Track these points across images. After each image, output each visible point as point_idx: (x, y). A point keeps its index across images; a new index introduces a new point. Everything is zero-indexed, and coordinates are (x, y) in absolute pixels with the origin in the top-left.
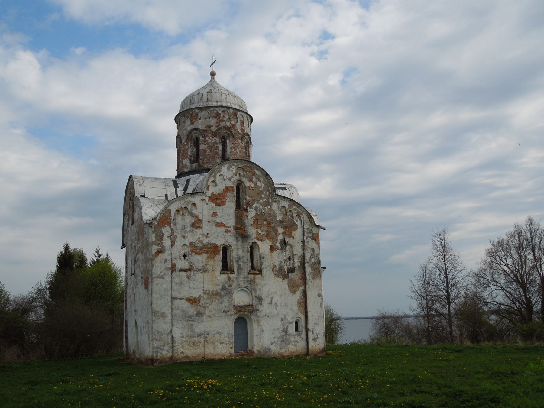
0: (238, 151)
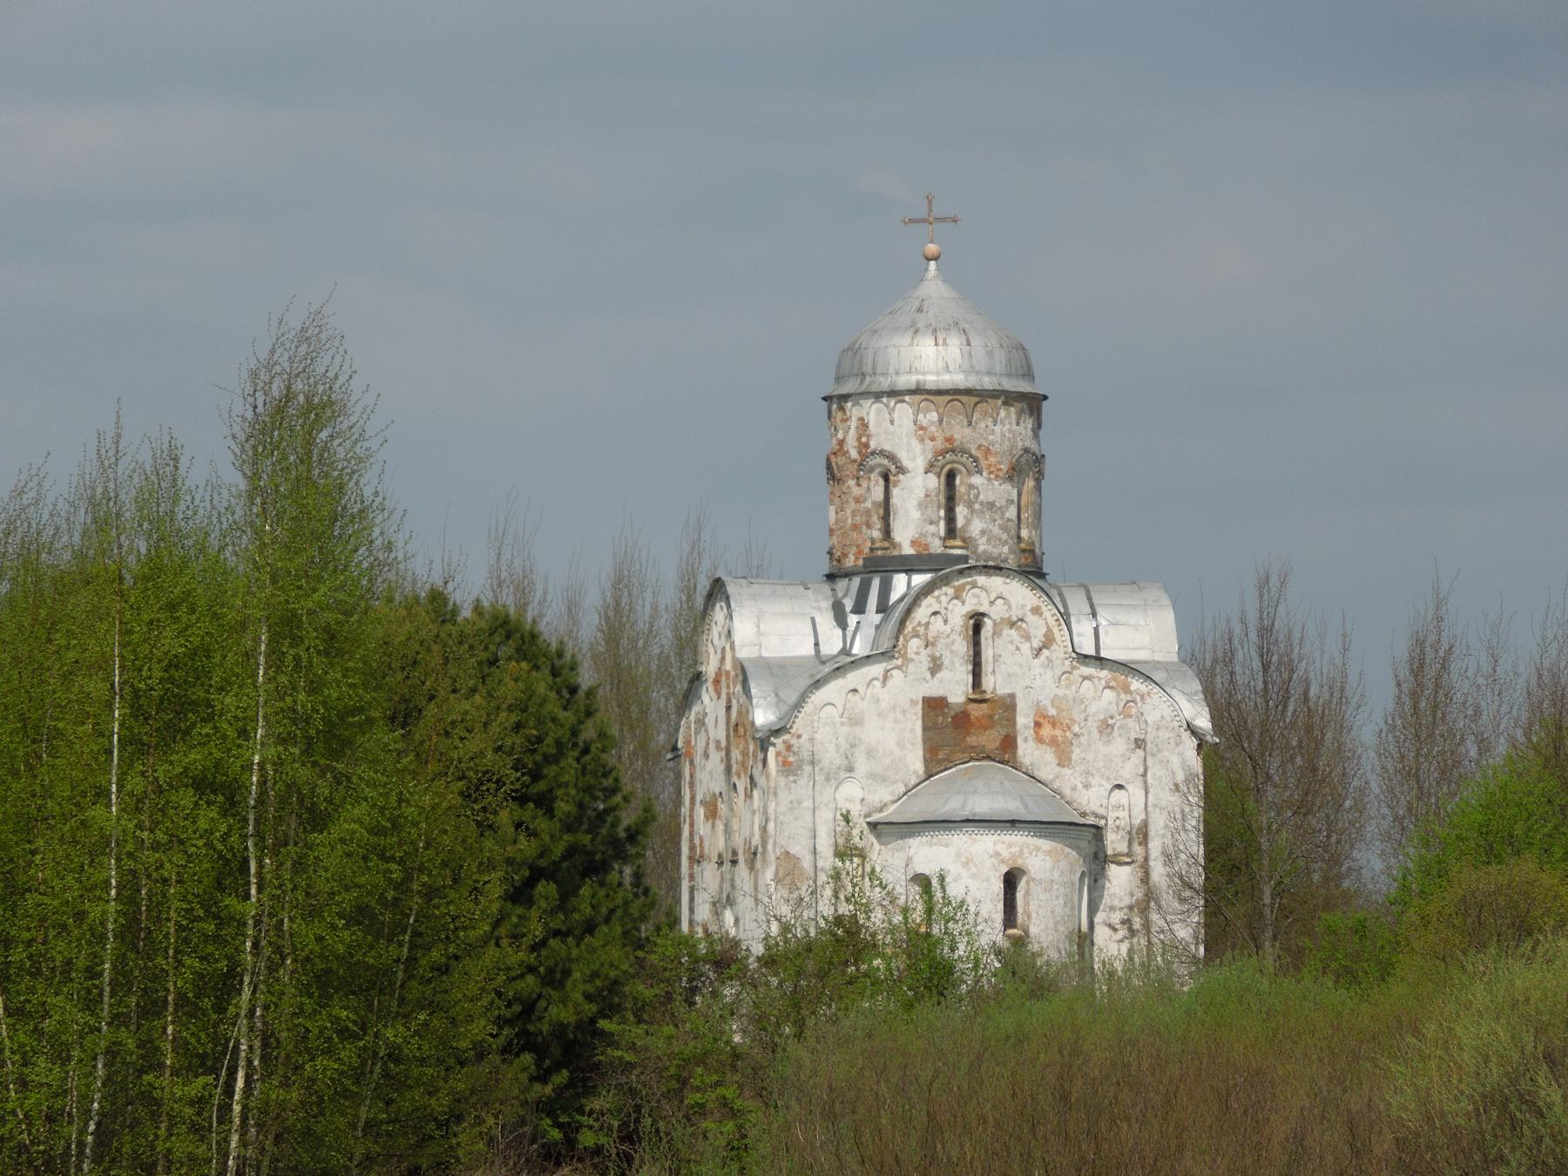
0: (849, 512)
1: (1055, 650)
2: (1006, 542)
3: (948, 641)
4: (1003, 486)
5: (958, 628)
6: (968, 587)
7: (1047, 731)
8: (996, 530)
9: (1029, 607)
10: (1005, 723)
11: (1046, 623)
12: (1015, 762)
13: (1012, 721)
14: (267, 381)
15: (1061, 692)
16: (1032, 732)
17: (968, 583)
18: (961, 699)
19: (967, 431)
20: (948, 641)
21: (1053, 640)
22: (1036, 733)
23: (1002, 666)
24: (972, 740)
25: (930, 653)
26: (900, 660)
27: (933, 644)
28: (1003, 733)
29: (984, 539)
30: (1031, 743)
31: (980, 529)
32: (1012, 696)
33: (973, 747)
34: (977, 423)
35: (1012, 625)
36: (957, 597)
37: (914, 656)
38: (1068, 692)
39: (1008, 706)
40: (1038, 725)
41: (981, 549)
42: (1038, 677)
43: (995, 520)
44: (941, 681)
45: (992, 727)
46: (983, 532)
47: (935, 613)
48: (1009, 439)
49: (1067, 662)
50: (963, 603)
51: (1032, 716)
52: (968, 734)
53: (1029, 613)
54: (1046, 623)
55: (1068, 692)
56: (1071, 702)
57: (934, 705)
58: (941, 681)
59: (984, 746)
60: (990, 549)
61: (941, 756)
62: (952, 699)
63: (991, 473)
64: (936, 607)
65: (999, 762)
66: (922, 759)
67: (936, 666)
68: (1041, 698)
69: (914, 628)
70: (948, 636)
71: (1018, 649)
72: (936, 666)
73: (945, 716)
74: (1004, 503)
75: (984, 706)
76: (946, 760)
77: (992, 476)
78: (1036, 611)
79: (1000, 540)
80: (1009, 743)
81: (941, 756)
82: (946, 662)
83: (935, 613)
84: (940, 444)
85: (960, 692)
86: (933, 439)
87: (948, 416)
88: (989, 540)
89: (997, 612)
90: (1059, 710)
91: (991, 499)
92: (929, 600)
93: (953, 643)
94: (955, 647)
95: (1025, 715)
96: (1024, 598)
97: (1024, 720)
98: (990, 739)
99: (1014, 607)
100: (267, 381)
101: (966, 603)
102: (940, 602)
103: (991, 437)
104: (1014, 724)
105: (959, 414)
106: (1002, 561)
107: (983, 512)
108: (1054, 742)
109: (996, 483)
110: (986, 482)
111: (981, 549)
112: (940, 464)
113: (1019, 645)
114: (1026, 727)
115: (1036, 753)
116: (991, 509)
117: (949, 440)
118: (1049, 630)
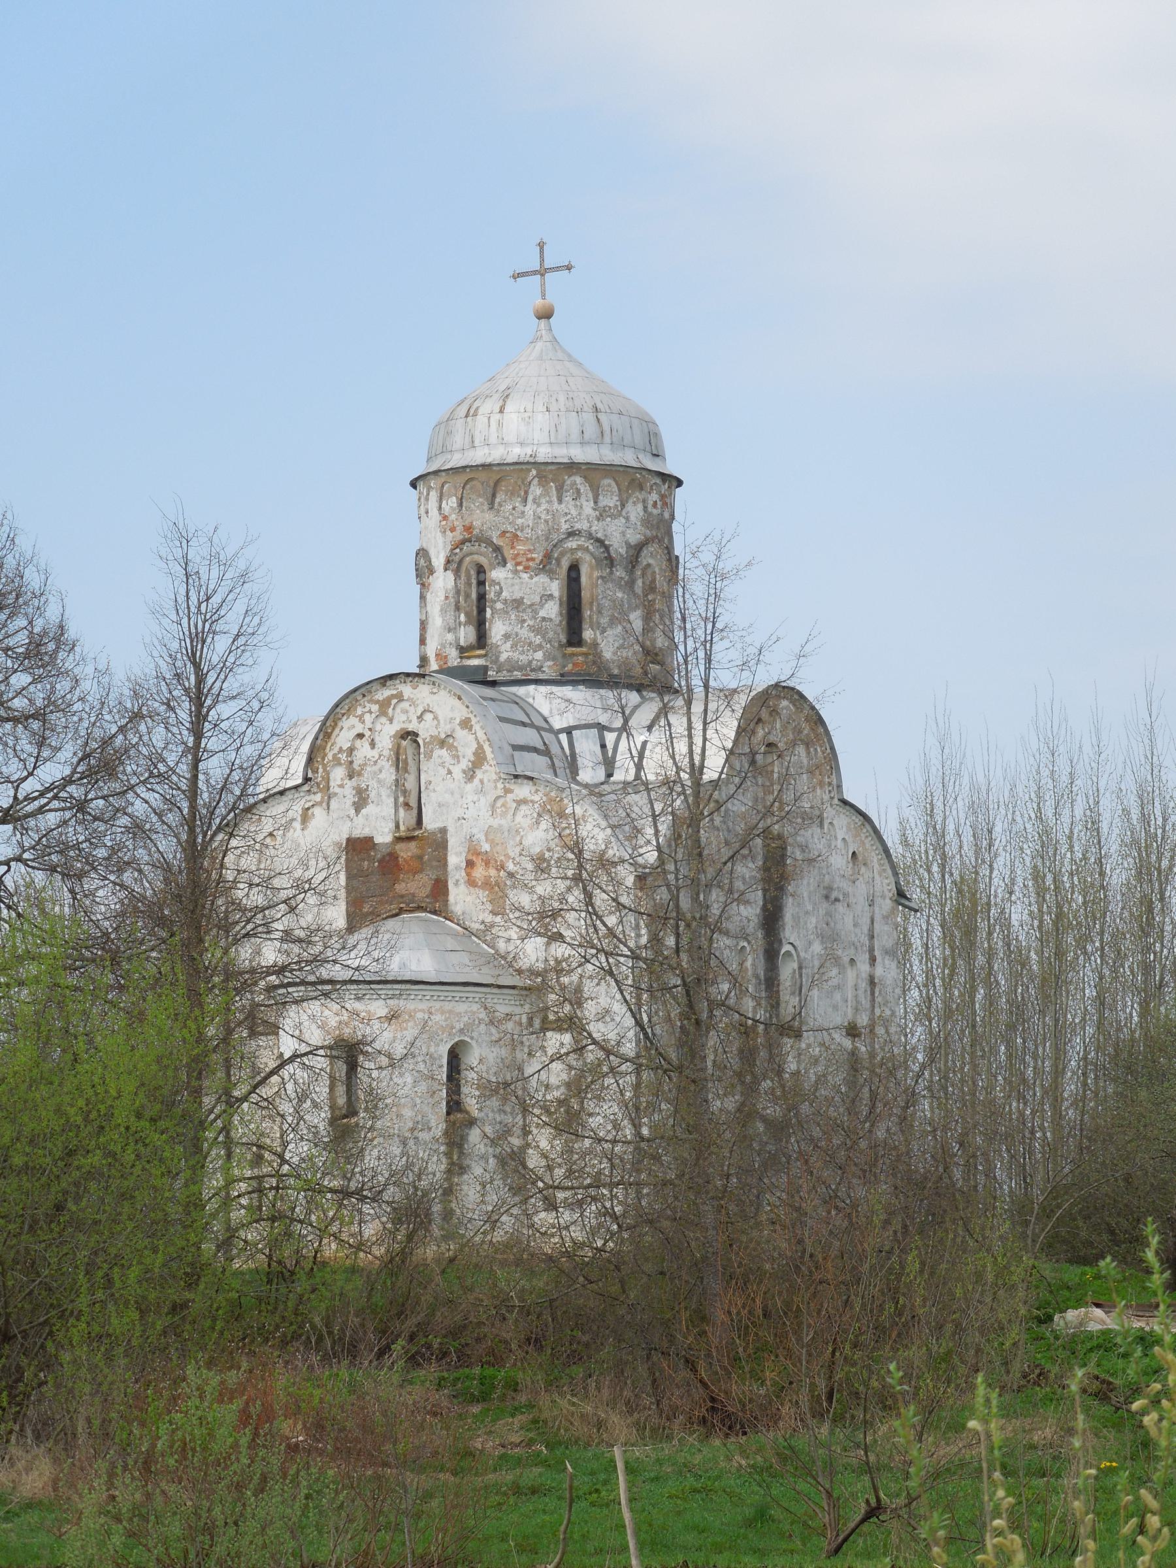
1: (487, 771)
2: (540, 647)
3: (376, 768)
4: (536, 579)
5: (386, 753)
6: (394, 701)
7: (479, 872)
8: (524, 633)
9: (458, 721)
10: (435, 863)
11: (476, 739)
12: (446, 911)
13: (443, 862)
14: (618, 546)
15: (495, 822)
16: (464, 874)
17: (393, 696)
18: (388, 839)
19: (489, 516)
20: (376, 768)
21: (485, 759)
22: (468, 874)
23: (432, 794)
24: (400, 888)
25: (355, 784)
26: (319, 795)
27: (360, 774)
28: (434, 877)
29: (509, 644)
30: (463, 888)
31: (503, 633)
32: (444, 831)
33: (402, 896)
34: (500, 505)
35: (442, 743)
36: (383, 712)
37: (337, 790)
38: (503, 822)
39: (439, 843)
40: (470, 864)
41: (503, 657)
42: (471, 805)
43: (524, 621)
44: (367, 817)
45: (421, 871)
46: (507, 636)
47: (360, 736)
48: (546, 521)
49: (500, 785)
50: (391, 720)
51: (464, 855)
52: (396, 881)
53: (458, 728)
54: (476, 739)
55: (503, 822)
56: (506, 833)
57: (358, 847)
58: (367, 817)
59: (413, 895)
60: (516, 656)
61: (366, 909)
62: (378, 840)
63: (518, 564)
64: (359, 729)
65: (430, 912)
66: (345, 913)
67: (361, 801)
68: (475, 831)
69: (335, 755)
70: (376, 761)
71: (450, 772)
72: (361, 801)
73: (371, 860)
74: (537, 599)
75: (413, 844)
76: (372, 913)
77: (520, 568)
78: (466, 724)
79: (530, 644)
80: (440, 889)
81: (366, 909)
82: (373, 795)
83: (360, 736)
84: (458, 535)
85: (387, 830)
86: (453, 530)
87: (467, 500)
88: (514, 646)
89: (426, 730)
90: (493, 843)
91: (517, 595)
92: (346, 723)
93: (381, 771)
94: (382, 776)
95: (456, 854)
96: (452, 709)
97: (455, 859)
98: (417, 886)
99: (442, 722)
100: (618, 546)
101: (395, 721)
102: (363, 722)
103: (519, 521)
104: (445, 864)
105: (479, 496)
106: (532, 670)
107: (507, 613)
108: (487, 884)
109: (525, 576)
110: (510, 576)
111: (503, 657)
112: (457, 558)
113: (451, 767)
114: (457, 868)
115: (469, 899)
116: (517, 608)
117: (468, 529)
118: (480, 747)
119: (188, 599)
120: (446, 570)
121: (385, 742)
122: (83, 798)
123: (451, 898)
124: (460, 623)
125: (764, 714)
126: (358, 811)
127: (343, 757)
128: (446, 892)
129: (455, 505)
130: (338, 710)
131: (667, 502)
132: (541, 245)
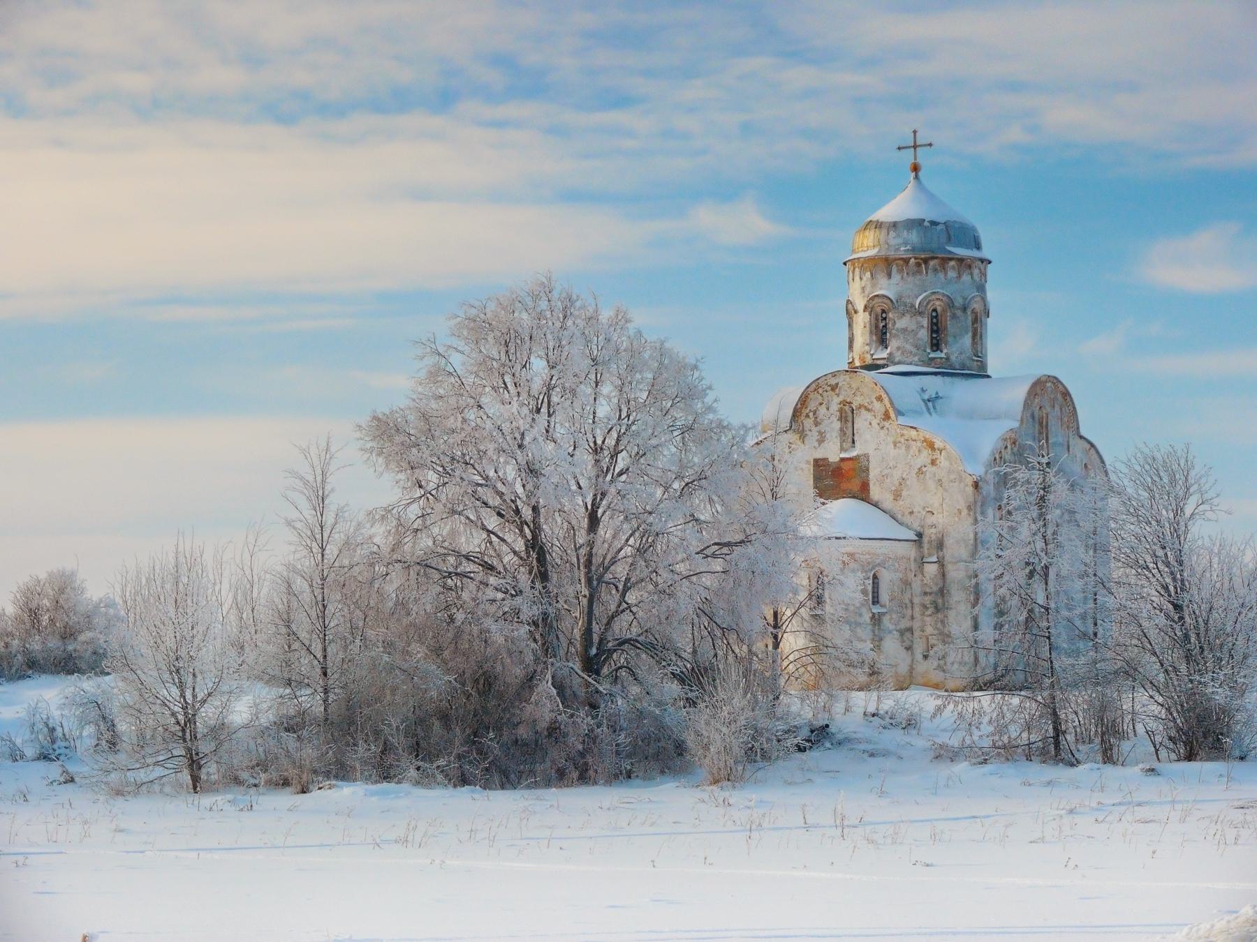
8: (908, 347)
46: (898, 348)
67: (821, 440)
82: (828, 436)
88: (903, 353)
101: (840, 396)
119: (343, 467)
120: (864, 311)
121: (835, 407)
122: (710, 404)
123: (872, 493)
124: (873, 341)
125: (1039, 391)
126: (820, 445)
127: (811, 414)
128: (868, 491)
129: (870, 276)
130: (808, 389)
131: (984, 274)
132: (915, 132)
